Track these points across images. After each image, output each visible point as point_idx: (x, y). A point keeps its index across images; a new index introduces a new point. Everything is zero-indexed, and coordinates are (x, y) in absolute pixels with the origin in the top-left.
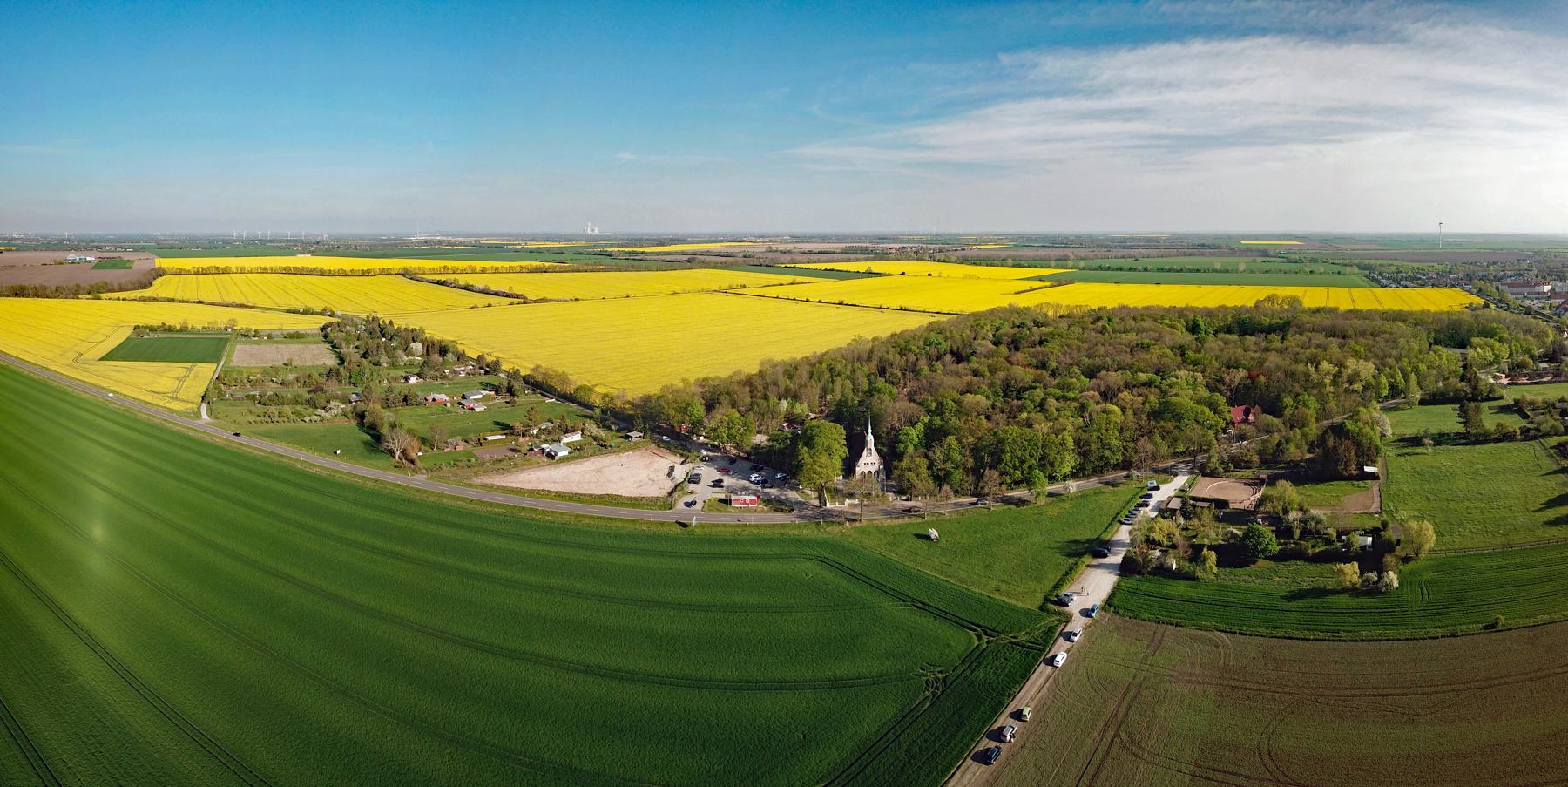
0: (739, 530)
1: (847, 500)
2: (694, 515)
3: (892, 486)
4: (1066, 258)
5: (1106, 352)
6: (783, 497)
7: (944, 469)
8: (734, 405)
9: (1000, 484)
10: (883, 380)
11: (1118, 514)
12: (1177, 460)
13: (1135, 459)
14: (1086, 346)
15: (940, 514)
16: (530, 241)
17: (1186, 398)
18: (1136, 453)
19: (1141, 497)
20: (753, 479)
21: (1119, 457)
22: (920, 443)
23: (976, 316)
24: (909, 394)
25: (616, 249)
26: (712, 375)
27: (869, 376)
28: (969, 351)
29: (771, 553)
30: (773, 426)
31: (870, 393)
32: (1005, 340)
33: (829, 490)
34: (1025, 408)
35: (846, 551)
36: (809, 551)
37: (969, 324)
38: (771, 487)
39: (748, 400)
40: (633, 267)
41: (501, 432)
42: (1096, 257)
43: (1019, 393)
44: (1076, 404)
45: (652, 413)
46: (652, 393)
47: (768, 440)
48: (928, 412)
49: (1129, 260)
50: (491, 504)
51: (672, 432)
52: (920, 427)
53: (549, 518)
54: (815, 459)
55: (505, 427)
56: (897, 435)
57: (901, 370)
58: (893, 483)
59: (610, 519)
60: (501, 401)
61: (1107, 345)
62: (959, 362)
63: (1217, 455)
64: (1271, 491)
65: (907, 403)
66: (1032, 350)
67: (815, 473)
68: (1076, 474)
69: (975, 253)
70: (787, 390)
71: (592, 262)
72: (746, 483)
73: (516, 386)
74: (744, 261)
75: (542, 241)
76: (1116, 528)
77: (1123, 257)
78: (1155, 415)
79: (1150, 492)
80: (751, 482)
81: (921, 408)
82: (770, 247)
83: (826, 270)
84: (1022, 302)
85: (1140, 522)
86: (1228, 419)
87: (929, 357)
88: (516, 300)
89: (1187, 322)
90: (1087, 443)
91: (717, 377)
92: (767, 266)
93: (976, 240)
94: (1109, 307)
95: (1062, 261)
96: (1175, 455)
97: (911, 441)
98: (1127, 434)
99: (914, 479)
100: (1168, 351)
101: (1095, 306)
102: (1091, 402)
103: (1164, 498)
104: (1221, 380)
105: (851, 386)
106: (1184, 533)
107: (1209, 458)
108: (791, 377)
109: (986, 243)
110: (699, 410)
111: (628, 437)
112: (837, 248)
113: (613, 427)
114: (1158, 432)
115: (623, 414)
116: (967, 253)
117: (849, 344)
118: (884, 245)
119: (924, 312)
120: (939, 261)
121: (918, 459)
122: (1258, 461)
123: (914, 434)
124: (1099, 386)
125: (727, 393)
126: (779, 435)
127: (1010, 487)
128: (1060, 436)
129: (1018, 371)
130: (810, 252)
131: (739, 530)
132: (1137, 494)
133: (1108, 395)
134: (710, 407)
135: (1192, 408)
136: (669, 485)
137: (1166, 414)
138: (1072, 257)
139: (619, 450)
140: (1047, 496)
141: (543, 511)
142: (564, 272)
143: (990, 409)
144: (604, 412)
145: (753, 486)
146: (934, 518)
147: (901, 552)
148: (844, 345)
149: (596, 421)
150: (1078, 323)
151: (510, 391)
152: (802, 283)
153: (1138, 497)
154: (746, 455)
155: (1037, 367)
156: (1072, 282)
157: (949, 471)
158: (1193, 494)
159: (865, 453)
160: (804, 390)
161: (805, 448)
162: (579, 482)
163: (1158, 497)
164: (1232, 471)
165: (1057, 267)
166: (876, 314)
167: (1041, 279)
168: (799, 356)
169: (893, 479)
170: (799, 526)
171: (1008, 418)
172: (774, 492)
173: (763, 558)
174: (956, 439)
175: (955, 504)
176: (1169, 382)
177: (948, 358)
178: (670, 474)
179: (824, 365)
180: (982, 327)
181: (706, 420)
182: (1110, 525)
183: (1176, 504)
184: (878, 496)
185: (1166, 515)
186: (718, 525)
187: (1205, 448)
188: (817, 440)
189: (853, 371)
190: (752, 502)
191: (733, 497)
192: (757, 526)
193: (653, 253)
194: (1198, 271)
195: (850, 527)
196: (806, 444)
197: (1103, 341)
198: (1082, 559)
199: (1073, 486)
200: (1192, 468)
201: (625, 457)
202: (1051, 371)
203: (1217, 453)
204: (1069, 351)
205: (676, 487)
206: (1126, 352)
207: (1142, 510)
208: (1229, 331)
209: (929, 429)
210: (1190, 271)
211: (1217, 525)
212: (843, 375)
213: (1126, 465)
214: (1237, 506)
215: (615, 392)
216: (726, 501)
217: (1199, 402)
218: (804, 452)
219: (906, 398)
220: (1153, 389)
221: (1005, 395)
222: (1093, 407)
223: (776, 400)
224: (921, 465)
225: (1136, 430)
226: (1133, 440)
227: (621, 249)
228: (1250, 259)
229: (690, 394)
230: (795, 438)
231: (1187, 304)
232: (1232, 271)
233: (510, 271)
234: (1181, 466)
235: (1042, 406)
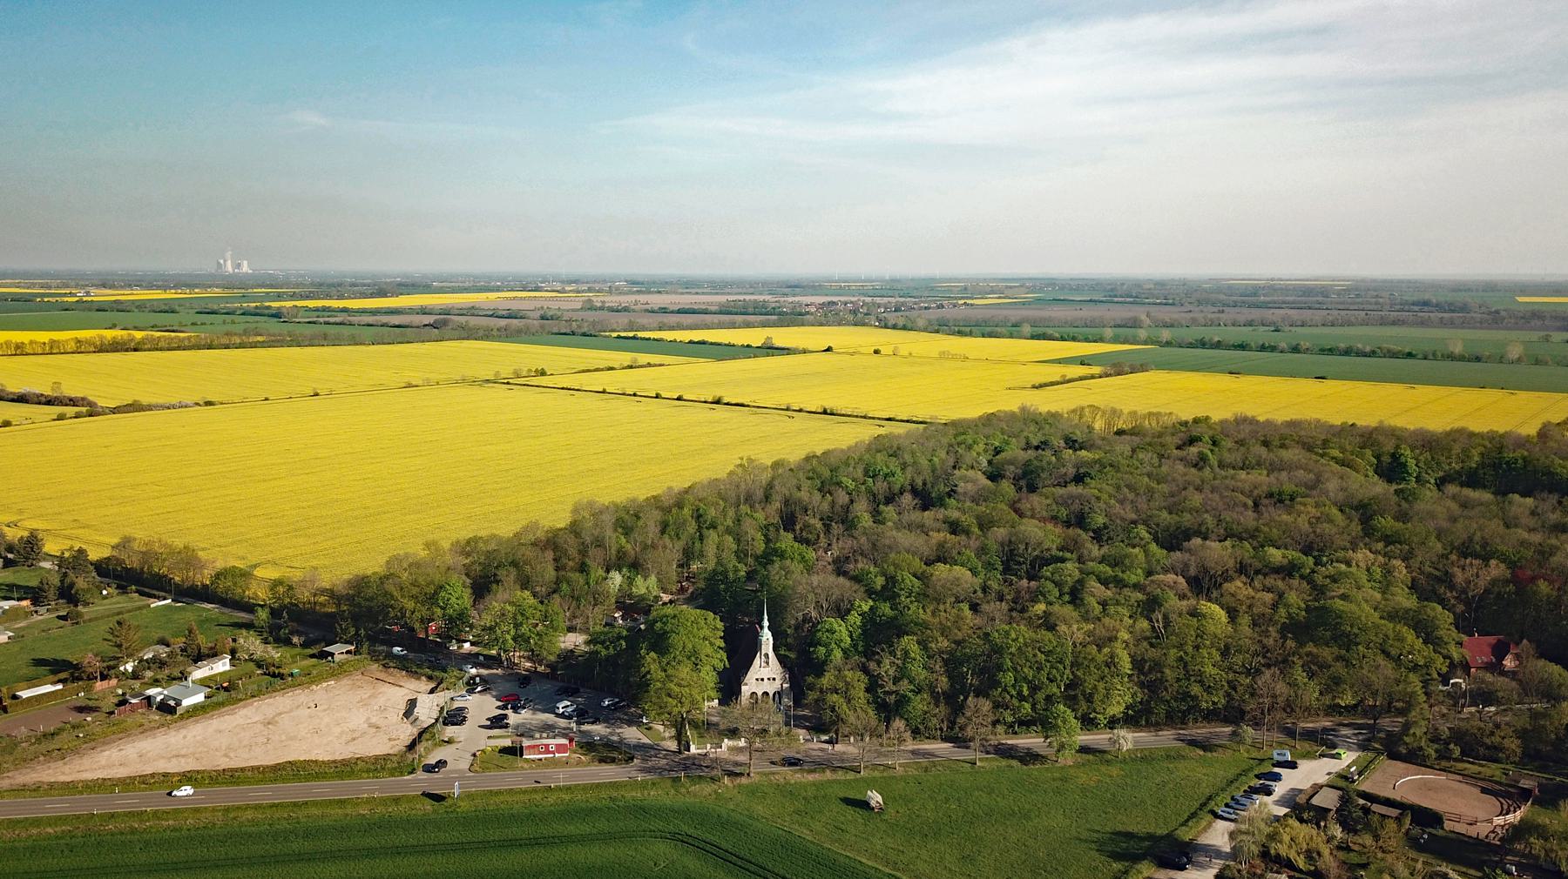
0: (538, 797)
1: (726, 740)
2: (456, 779)
3: (805, 718)
4: (1135, 324)
5: (1204, 504)
6: (615, 738)
7: (896, 692)
8: (525, 583)
9: (995, 723)
10: (790, 536)
11: (1210, 798)
12: (1338, 719)
13: (1251, 705)
14: (1164, 488)
15: (888, 767)
16: (97, 286)
17: (1365, 605)
18: (1252, 695)
19: (1258, 777)
20: (561, 711)
21: (1220, 699)
22: (855, 646)
23: (959, 428)
24: (836, 561)
25: (289, 304)
26: (483, 534)
27: (765, 528)
28: (942, 488)
29: (595, 831)
30: (595, 617)
31: (766, 558)
32: (1011, 470)
33: (695, 725)
34: (1044, 596)
35: (725, 824)
36: (660, 825)
37: (945, 441)
38: (593, 723)
39: (550, 573)
40: (325, 337)
41: (52, 678)
42: (1194, 321)
43: (1033, 567)
44: (1140, 596)
45: (370, 609)
46: (369, 572)
47: (588, 643)
48: (870, 593)
49: (1262, 329)
50: (37, 822)
51: (409, 638)
52: (855, 618)
53: (171, 822)
54: (670, 671)
55: (58, 668)
57: (821, 519)
58: (806, 712)
59: (295, 804)
60: (47, 616)
61: (1207, 488)
62: (925, 508)
63: (1423, 723)
64: (1544, 818)
65: (832, 578)
66: (1060, 491)
67: (670, 696)
68: (1134, 718)
69: (961, 313)
70: (621, 555)
71: (239, 328)
72: (549, 718)
73: (81, 583)
74: (542, 327)
75: (122, 287)
76: (1204, 823)
77: (1250, 324)
78: (1299, 630)
79: (1277, 770)
80: (558, 715)
81: (856, 587)
82: (590, 301)
83: (691, 342)
84: (1044, 403)
85: (1251, 820)
86: (1456, 656)
87: (874, 498)
88: (70, 410)
89: (1378, 457)
90: (1157, 666)
91: (494, 536)
92: (584, 335)
93: (966, 289)
94: (1216, 416)
95: (1126, 329)
96: (1333, 710)
97: (839, 643)
98: (1238, 660)
99: (843, 708)
100: (1335, 511)
101: (1187, 416)
102: (1171, 594)
103: (1306, 785)
104: (1447, 579)
105: (734, 547)
106: (1341, 855)
107: (1406, 727)
108: (627, 531)
109: (984, 293)
110: (459, 595)
111: (324, 655)
112: (711, 304)
113: (295, 640)
114: (1300, 662)
115: (314, 611)
116: (948, 313)
117: (731, 473)
118: (796, 299)
119: (865, 417)
120: (894, 327)
121: (849, 674)
122: (1518, 751)
123: (842, 631)
124: (1186, 565)
125: (514, 564)
126: (606, 634)
127: (1011, 729)
128: (1106, 650)
129: (1032, 530)
130: (664, 311)
131: (538, 797)
132: (1251, 769)
133: (1203, 583)
134: (482, 586)
135: (1376, 626)
136: (407, 732)
137: (1321, 631)
138: (1148, 321)
139: (308, 679)
140: (1078, 751)
141: (156, 812)
142: (178, 348)
143: (980, 594)
144: (275, 613)
145: (562, 722)
146: (876, 774)
147: (817, 826)
148: (722, 474)
149: (260, 633)
150: (1150, 444)
151: (68, 594)
152: (649, 365)
153: (1251, 775)
154: (548, 671)
155: (1068, 524)
156: (1143, 368)
158: (1366, 786)
159: (757, 661)
160: (650, 555)
161: (653, 654)
162: (229, 748)
163: (1290, 781)
164: (1456, 760)
165: (1116, 340)
166: (781, 421)
167: (1083, 361)
168: (642, 495)
169: (806, 706)
170: (643, 786)
171: (1011, 610)
172: (598, 730)
173: (582, 840)
174: (919, 643)
175: (913, 752)
176: (1331, 570)
177: (907, 499)
178: (408, 713)
179: (687, 511)
180: (970, 448)
181: (474, 613)
182: (1193, 815)
183: (1328, 799)
184: (779, 735)
185: (1305, 816)
186: (499, 793)
187: (1400, 705)
188: (674, 639)
189: (738, 521)
190: (560, 748)
191: (526, 743)
192: (568, 788)
193: (363, 311)
194: (1410, 355)
195: (730, 784)
196: (652, 648)
197: (1198, 481)
198: (1139, 866)
199: (1128, 739)
200: (1369, 740)
201: (319, 692)
202: (1094, 531)
203: (1427, 719)
204: (1131, 496)
205: (420, 735)
206: (1245, 505)
207: (1260, 799)
208: (1472, 480)
209: (870, 619)
210: (1394, 355)
211: (1412, 854)
212: (720, 528)
213: (1233, 715)
214: (1461, 828)
215: (296, 575)
216: (514, 751)
217: (1393, 616)
218: (651, 661)
219: (830, 568)
220: (1295, 582)
221: (1007, 570)
222: (1173, 603)
223: (601, 572)
224: (856, 684)
225: (1256, 654)
226: (1248, 673)
227: (299, 303)
228: (1535, 336)
229: (443, 569)
230: (634, 637)
231: (1381, 422)
232: (1489, 359)
233: (52, 349)
234: (1345, 731)
235: (1075, 596)
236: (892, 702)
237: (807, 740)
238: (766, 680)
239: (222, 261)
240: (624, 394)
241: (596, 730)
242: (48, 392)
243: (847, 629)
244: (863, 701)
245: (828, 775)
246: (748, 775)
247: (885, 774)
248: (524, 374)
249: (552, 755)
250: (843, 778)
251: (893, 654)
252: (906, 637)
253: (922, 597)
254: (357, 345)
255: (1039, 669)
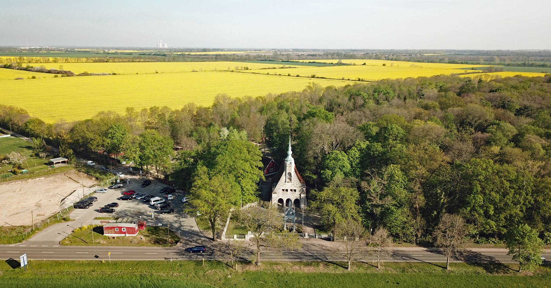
7: (382, 206)
20: (152, 203)
48: (368, 137)
52: (355, 153)
56: (324, 158)
97: (342, 168)
117: (305, 90)
121: (343, 190)
157: (388, 209)
159: (283, 178)
174: (402, 170)
175: (395, 254)
188: (219, 158)
190: (131, 231)
236: (379, 213)
237: (311, 237)
238: (289, 191)
239: (158, 44)
240: (276, 75)
241: (168, 218)
242: (58, 69)
243: (349, 159)
244: (354, 211)
245: (321, 269)
246: (256, 263)
247: (369, 272)
248: (239, 69)
249: (124, 235)
250: (333, 272)
251: (381, 175)
252: (392, 165)
253: (405, 140)
254: (185, 62)
255: (505, 195)
